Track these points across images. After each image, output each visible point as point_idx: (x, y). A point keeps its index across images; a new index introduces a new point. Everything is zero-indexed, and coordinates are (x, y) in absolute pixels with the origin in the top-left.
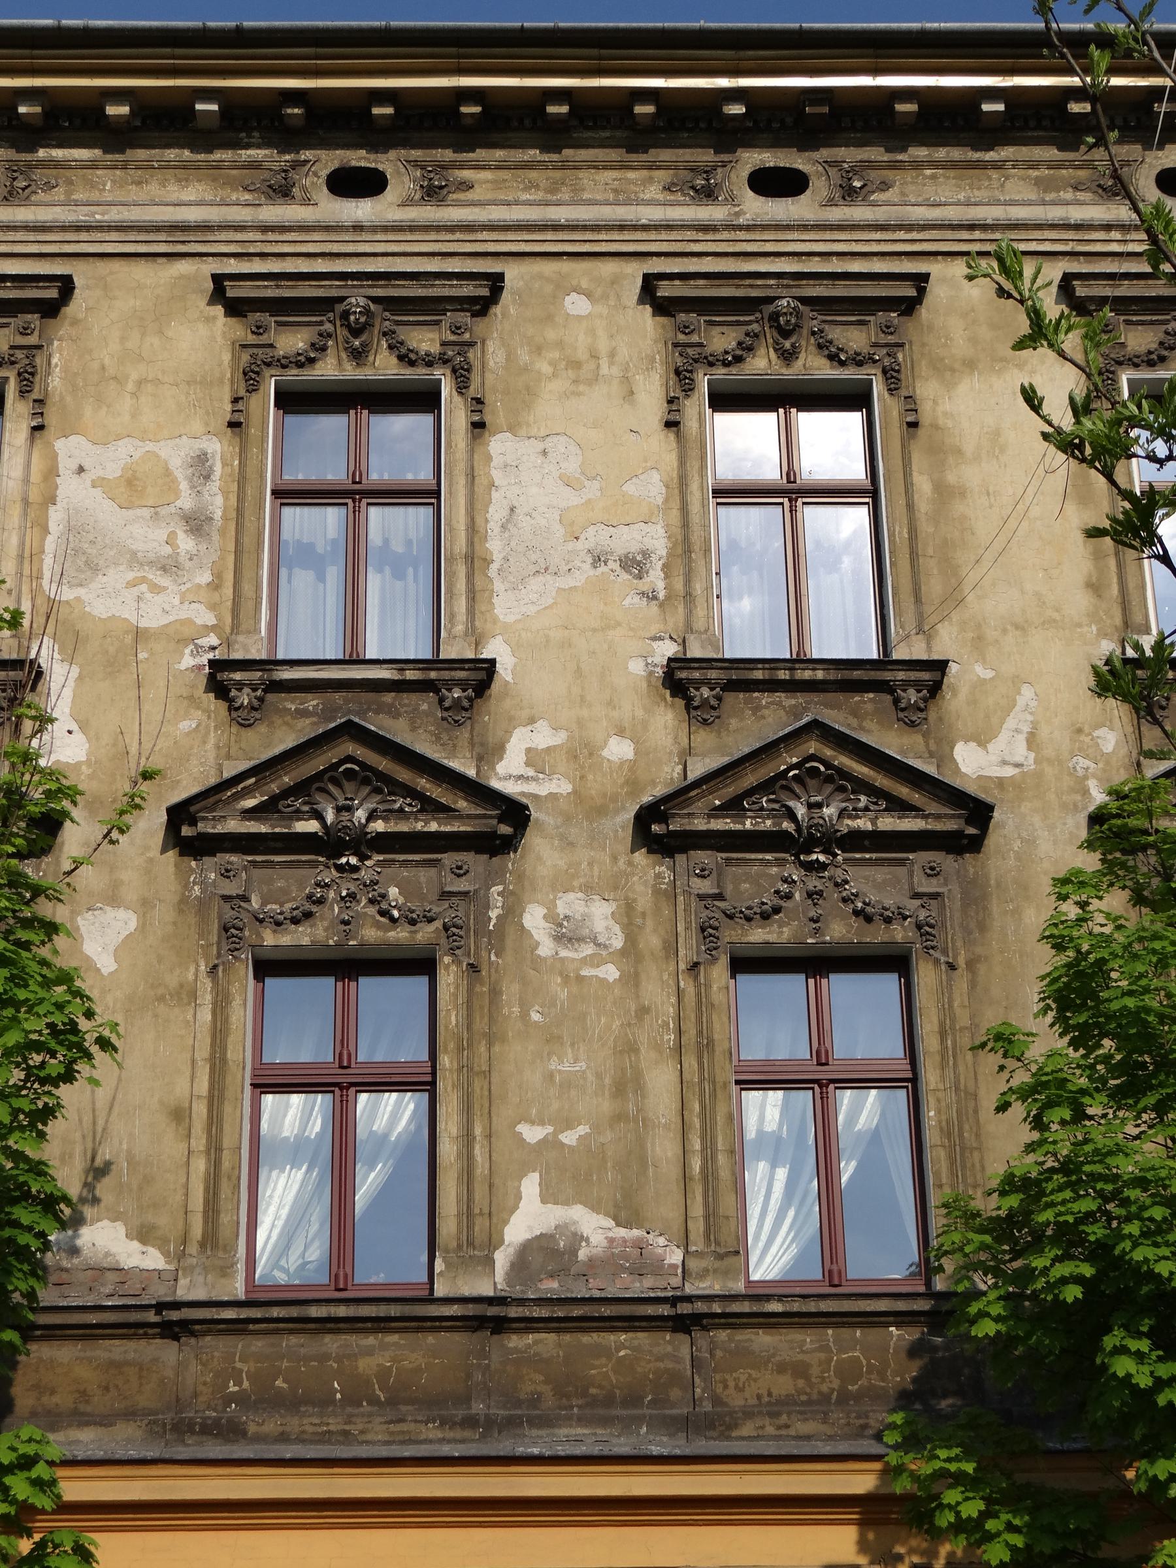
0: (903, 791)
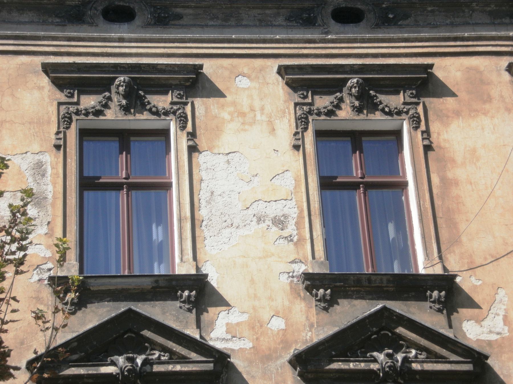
0: (437, 348)
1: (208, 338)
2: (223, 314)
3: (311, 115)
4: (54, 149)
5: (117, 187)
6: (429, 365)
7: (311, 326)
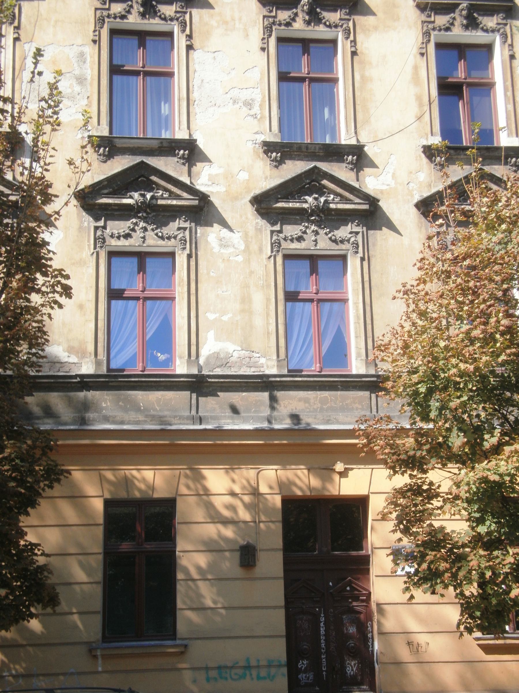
1: (194, 183)
2: (207, 168)
3: (275, 25)
4: (92, 43)
5: (136, 73)
6: (341, 205)
7: (266, 178)
